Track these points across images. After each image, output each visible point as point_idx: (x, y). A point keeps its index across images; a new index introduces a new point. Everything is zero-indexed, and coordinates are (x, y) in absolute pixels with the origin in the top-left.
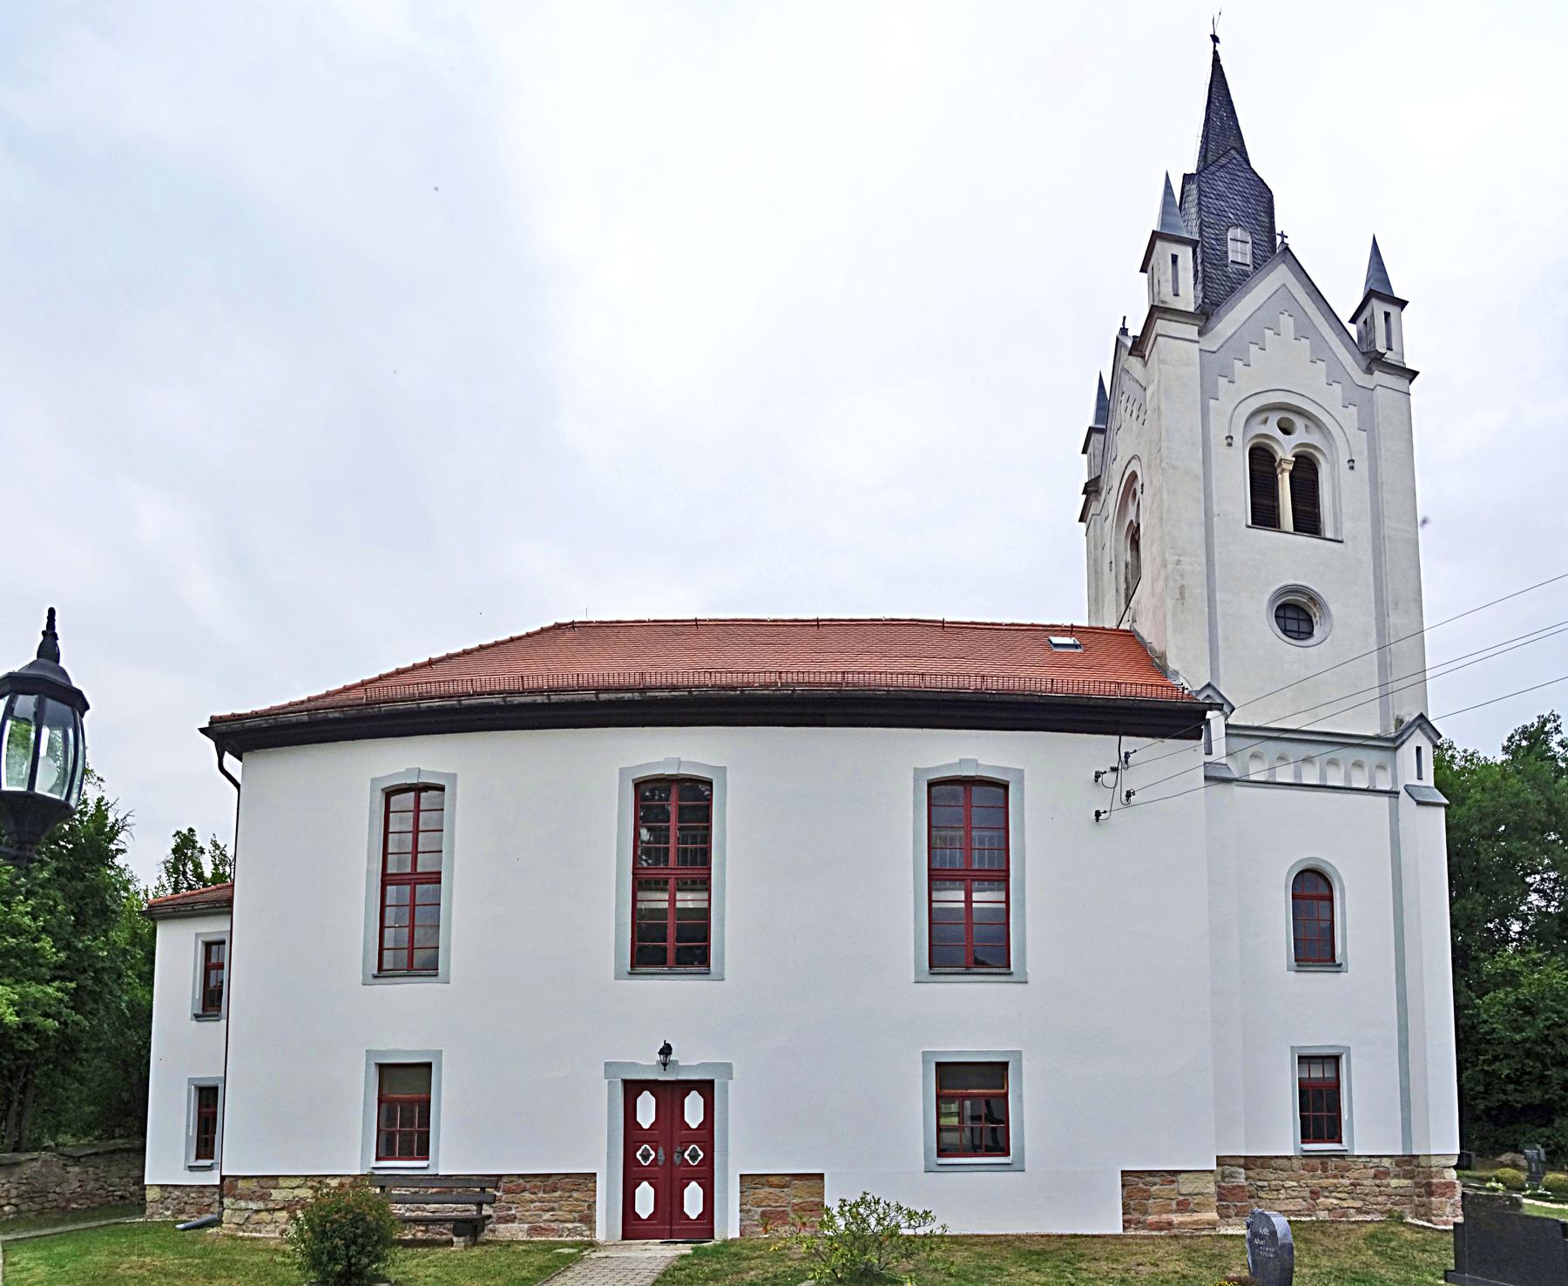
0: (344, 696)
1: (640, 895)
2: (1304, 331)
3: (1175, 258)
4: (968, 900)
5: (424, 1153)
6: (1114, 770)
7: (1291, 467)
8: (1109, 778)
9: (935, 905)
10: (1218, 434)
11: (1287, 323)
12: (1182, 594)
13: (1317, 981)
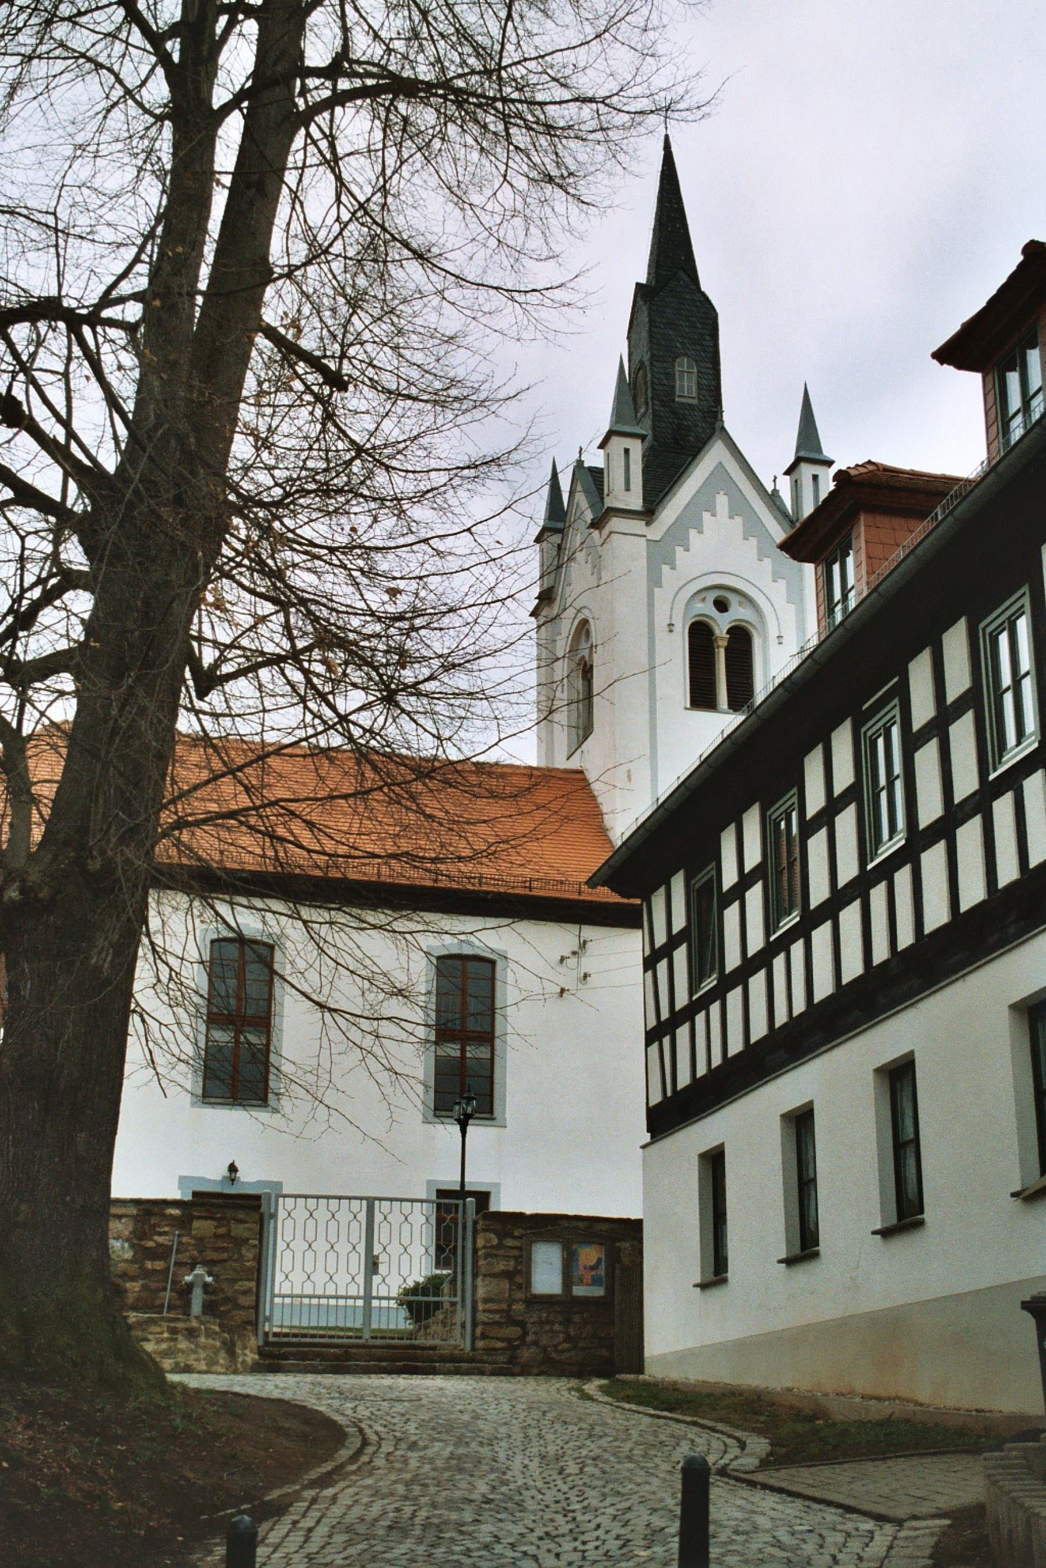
2: (739, 507)
3: (627, 451)
4: (463, 1051)
5: (642, 1373)
7: (725, 643)
8: (572, 962)
10: (661, 622)
11: (722, 501)
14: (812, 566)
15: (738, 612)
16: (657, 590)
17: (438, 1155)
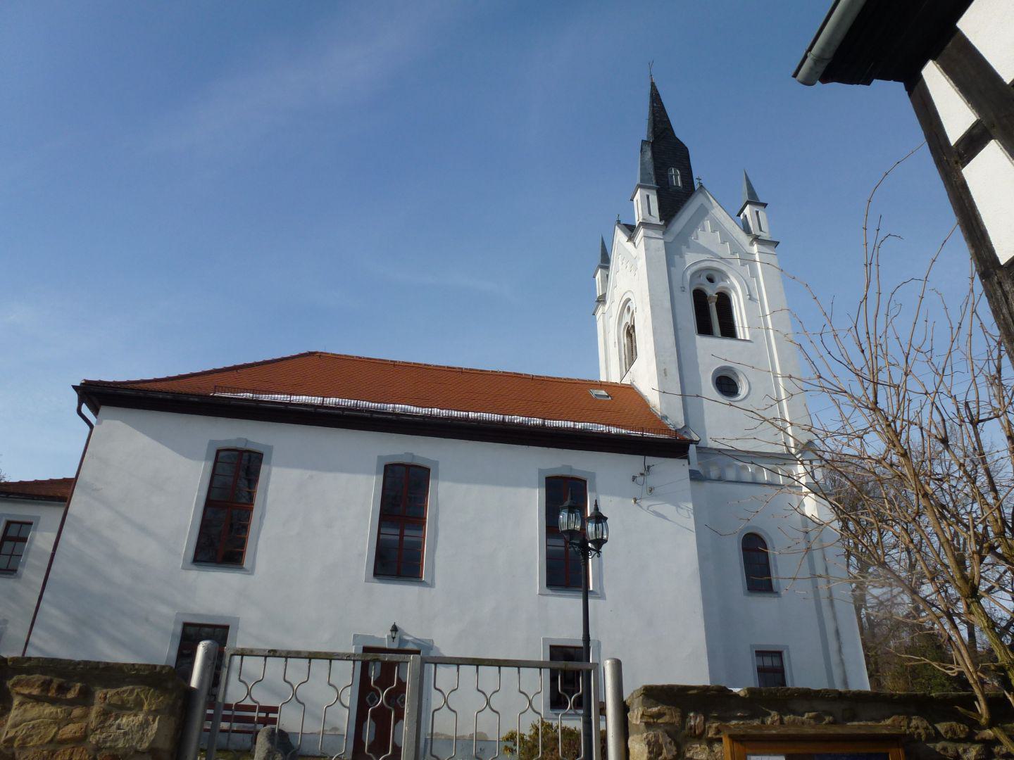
0: (141, 385)
1: (383, 531)
4: (402, 535)
6: (642, 474)
8: (640, 479)
9: (381, 537)
12: (665, 373)
13: (762, 603)
14: (601, 380)
15: (720, 285)
16: (672, 269)
17: (561, 618)
